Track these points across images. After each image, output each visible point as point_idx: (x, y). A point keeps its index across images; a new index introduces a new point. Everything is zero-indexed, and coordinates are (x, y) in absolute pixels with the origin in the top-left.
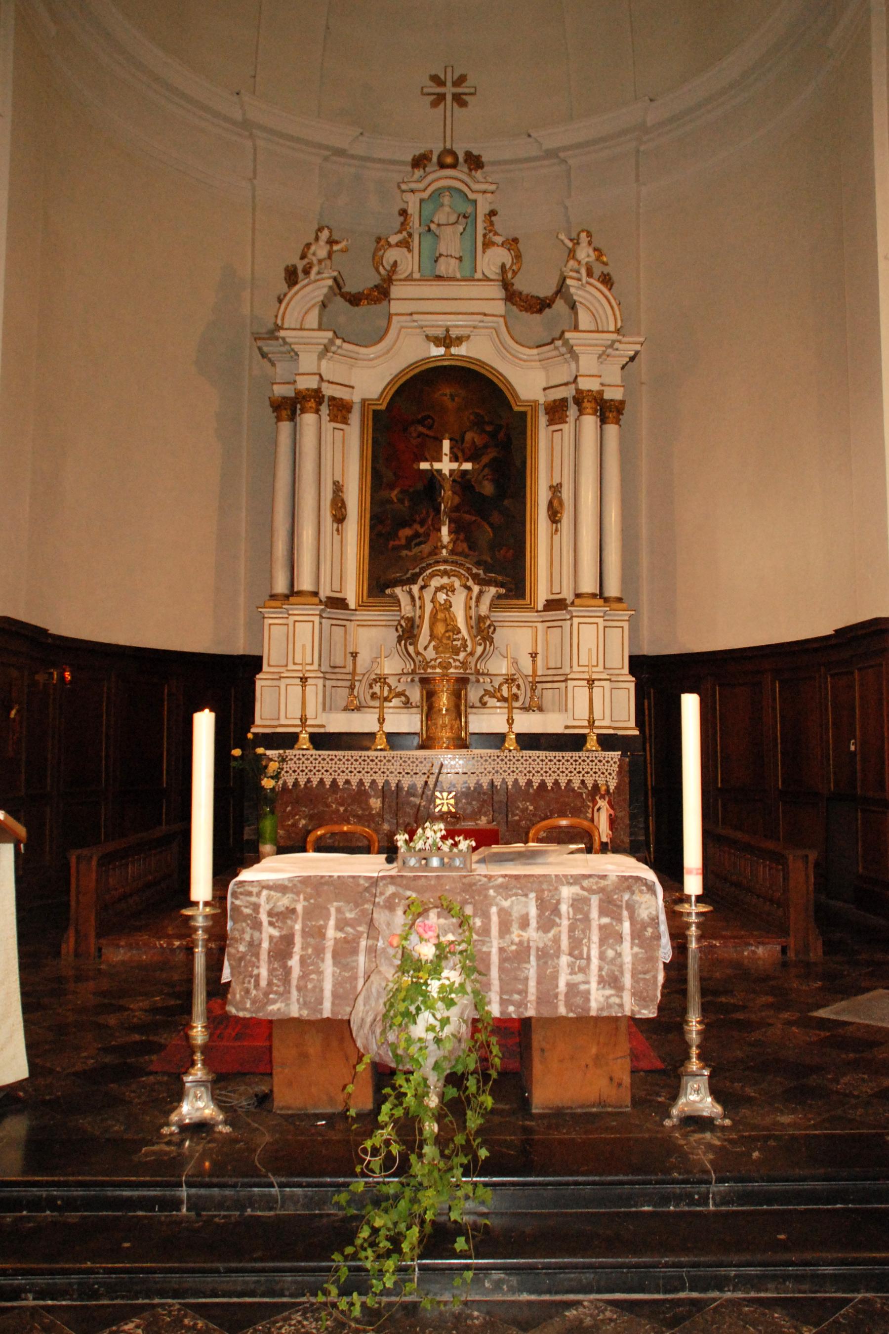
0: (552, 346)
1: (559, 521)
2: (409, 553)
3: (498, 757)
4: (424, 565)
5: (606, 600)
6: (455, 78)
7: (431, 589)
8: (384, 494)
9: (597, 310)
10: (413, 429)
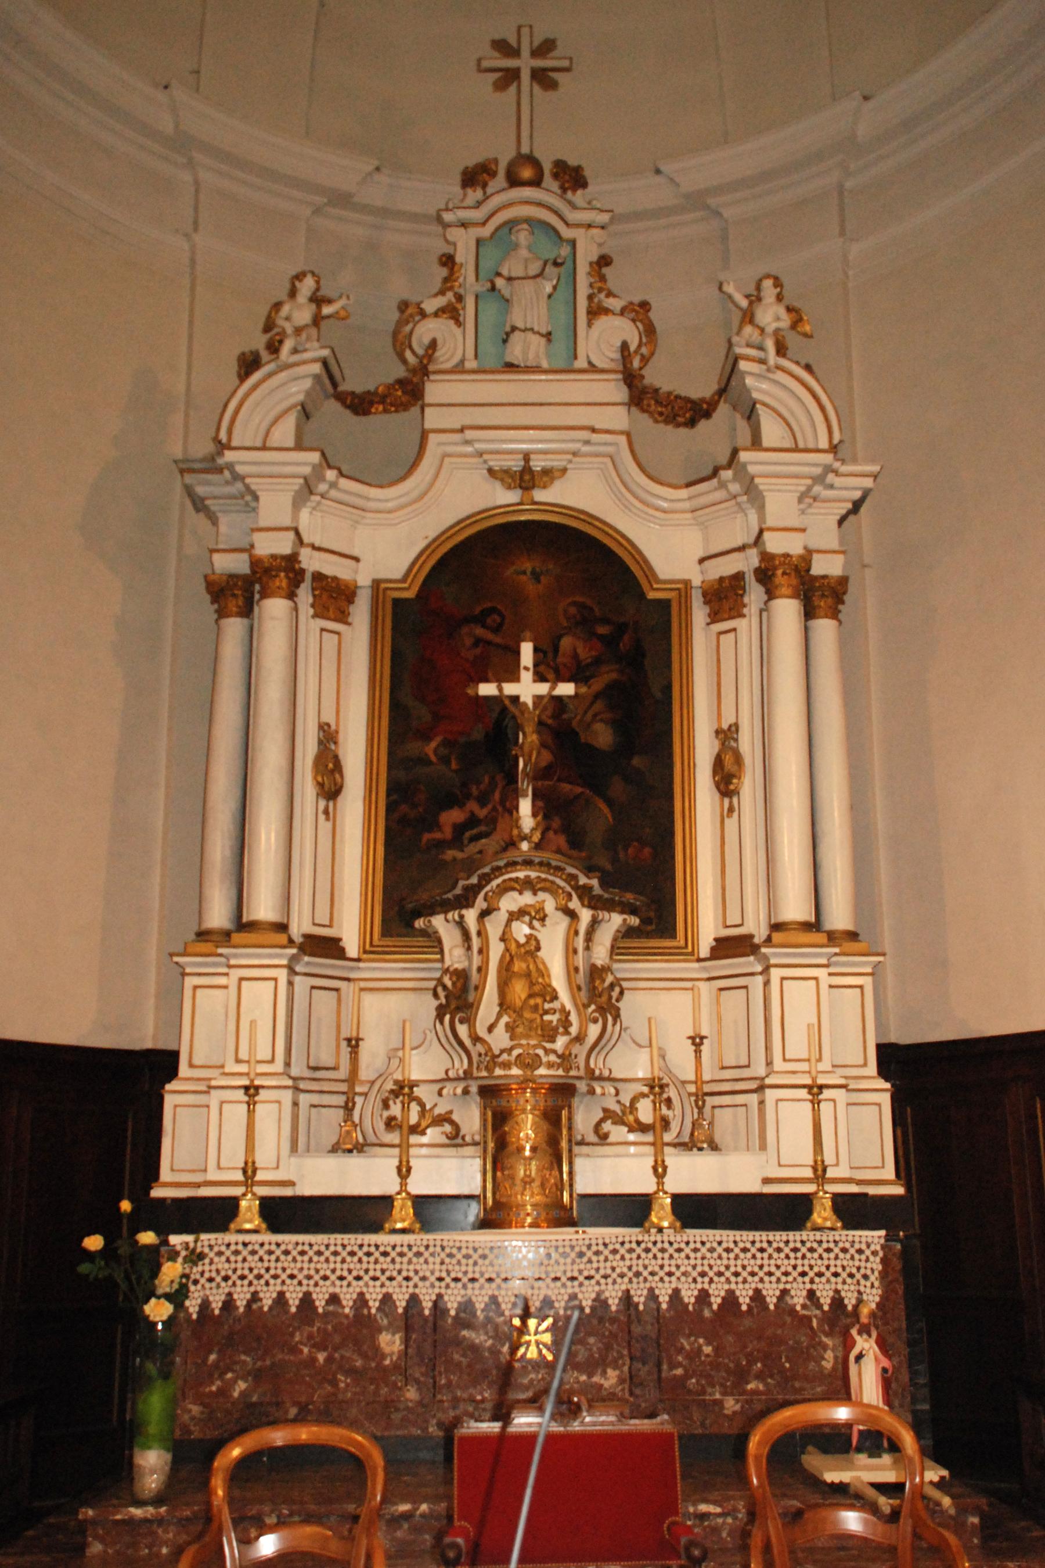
0: (715, 481)
1: (736, 792)
2: (460, 855)
3: (638, 1243)
4: (487, 870)
5: (832, 938)
6: (536, 44)
7: (501, 916)
8: (413, 748)
9: (792, 413)
10: (465, 630)
